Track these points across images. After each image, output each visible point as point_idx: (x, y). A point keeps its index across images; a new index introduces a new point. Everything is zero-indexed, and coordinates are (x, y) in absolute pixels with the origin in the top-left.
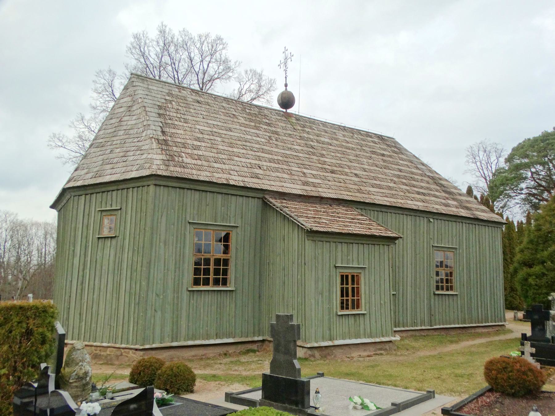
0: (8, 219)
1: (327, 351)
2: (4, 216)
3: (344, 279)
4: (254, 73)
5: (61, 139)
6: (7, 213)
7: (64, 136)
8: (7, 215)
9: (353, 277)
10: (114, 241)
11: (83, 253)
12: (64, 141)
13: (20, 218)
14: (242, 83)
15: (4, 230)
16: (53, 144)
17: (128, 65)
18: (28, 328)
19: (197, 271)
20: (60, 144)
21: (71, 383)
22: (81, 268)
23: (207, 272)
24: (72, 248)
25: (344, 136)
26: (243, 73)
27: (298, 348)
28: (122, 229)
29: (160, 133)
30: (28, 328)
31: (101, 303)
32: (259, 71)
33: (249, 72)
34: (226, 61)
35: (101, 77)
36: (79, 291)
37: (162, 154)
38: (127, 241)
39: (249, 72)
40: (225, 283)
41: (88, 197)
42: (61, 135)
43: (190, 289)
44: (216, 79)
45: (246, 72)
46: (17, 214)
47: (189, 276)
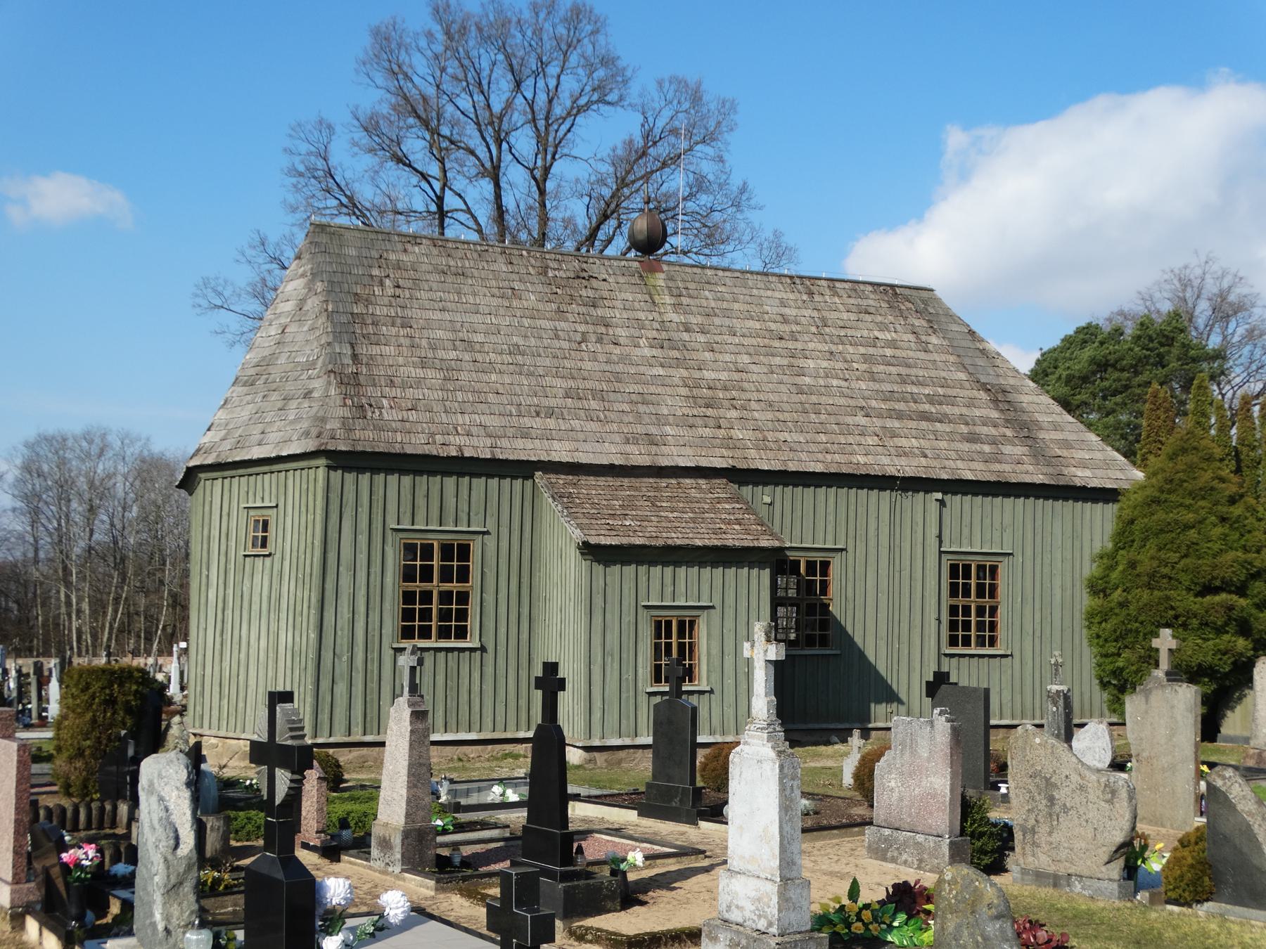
0: (128, 453)
1: (622, 754)
2: (119, 443)
3: (661, 628)
4: (680, 83)
5: (220, 289)
6: (127, 435)
7: (226, 282)
8: (127, 441)
9: (681, 624)
10: (268, 560)
11: (221, 581)
12: (226, 293)
13: (157, 447)
14: (649, 114)
15: (119, 478)
16: (204, 303)
17: (357, 107)
18: (111, 695)
19: (407, 615)
20: (219, 303)
21: (105, 712)
22: (220, 605)
23: (426, 615)
24: (205, 572)
25: (783, 303)
26: (652, 87)
27: (568, 748)
28: (280, 540)
29: (348, 361)
30: (111, 695)
31: (251, 667)
32: (692, 81)
33: (667, 85)
34: (607, 61)
35: (300, 138)
36: (218, 646)
37: (345, 405)
38: (287, 563)
39: (667, 85)
40: (462, 633)
41: (227, 481)
42: (221, 281)
43: (395, 645)
44: (577, 110)
45: (660, 84)
46: (148, 439)
47: (392, 623)
